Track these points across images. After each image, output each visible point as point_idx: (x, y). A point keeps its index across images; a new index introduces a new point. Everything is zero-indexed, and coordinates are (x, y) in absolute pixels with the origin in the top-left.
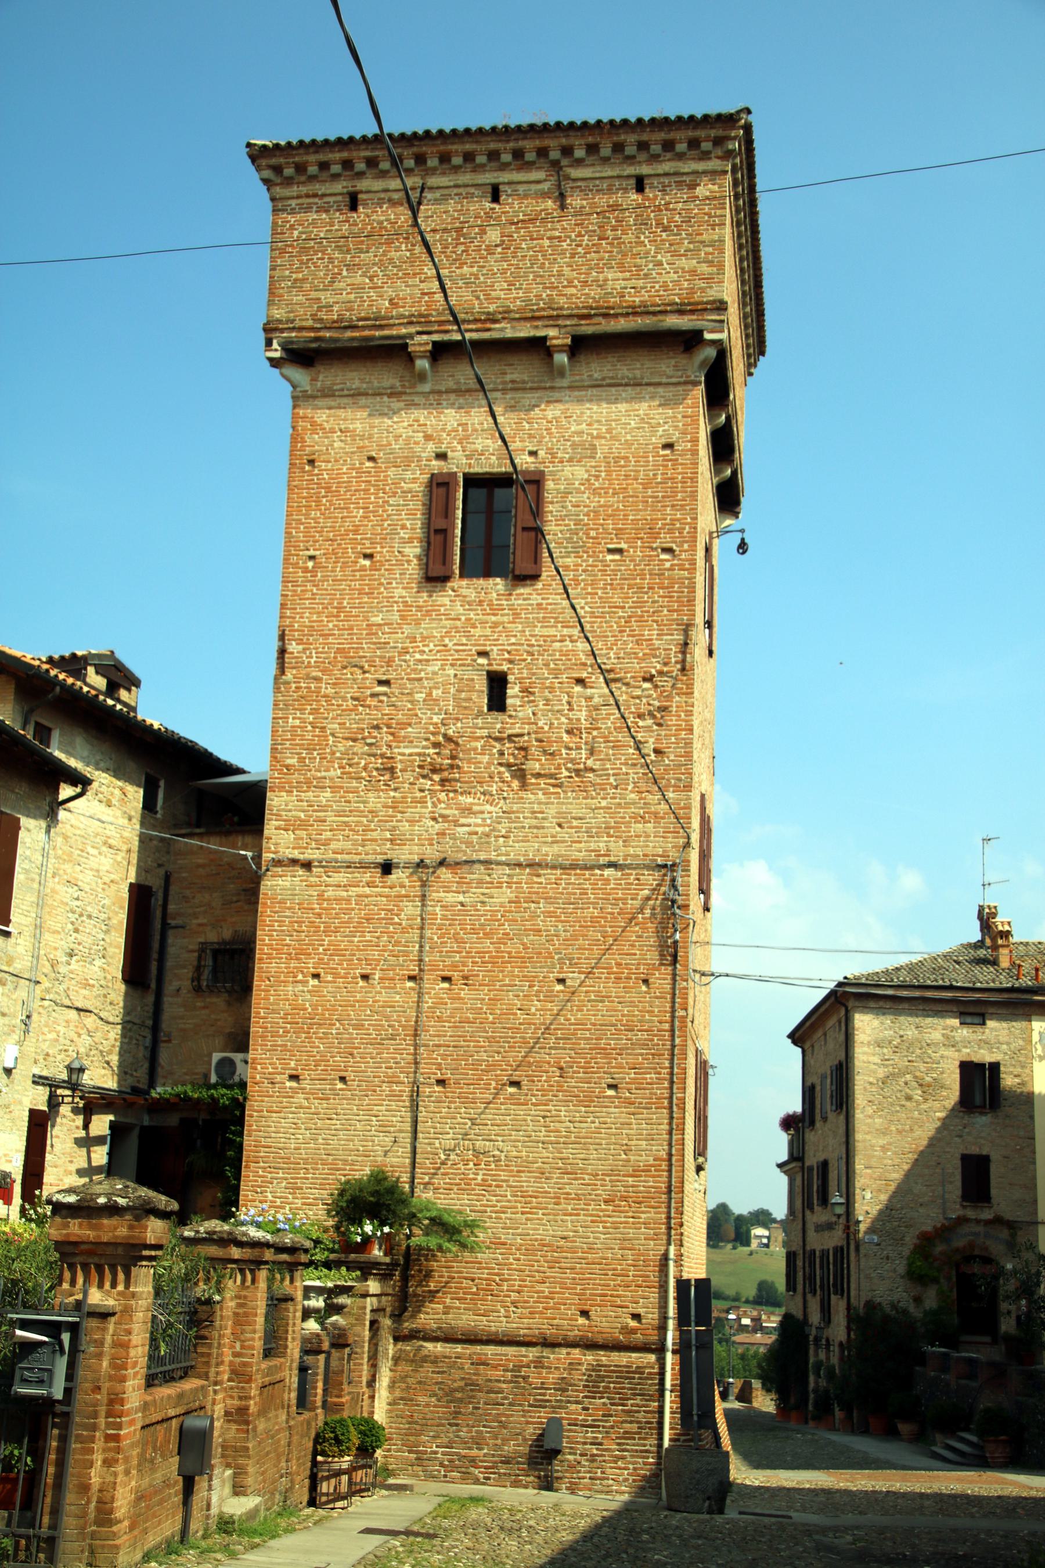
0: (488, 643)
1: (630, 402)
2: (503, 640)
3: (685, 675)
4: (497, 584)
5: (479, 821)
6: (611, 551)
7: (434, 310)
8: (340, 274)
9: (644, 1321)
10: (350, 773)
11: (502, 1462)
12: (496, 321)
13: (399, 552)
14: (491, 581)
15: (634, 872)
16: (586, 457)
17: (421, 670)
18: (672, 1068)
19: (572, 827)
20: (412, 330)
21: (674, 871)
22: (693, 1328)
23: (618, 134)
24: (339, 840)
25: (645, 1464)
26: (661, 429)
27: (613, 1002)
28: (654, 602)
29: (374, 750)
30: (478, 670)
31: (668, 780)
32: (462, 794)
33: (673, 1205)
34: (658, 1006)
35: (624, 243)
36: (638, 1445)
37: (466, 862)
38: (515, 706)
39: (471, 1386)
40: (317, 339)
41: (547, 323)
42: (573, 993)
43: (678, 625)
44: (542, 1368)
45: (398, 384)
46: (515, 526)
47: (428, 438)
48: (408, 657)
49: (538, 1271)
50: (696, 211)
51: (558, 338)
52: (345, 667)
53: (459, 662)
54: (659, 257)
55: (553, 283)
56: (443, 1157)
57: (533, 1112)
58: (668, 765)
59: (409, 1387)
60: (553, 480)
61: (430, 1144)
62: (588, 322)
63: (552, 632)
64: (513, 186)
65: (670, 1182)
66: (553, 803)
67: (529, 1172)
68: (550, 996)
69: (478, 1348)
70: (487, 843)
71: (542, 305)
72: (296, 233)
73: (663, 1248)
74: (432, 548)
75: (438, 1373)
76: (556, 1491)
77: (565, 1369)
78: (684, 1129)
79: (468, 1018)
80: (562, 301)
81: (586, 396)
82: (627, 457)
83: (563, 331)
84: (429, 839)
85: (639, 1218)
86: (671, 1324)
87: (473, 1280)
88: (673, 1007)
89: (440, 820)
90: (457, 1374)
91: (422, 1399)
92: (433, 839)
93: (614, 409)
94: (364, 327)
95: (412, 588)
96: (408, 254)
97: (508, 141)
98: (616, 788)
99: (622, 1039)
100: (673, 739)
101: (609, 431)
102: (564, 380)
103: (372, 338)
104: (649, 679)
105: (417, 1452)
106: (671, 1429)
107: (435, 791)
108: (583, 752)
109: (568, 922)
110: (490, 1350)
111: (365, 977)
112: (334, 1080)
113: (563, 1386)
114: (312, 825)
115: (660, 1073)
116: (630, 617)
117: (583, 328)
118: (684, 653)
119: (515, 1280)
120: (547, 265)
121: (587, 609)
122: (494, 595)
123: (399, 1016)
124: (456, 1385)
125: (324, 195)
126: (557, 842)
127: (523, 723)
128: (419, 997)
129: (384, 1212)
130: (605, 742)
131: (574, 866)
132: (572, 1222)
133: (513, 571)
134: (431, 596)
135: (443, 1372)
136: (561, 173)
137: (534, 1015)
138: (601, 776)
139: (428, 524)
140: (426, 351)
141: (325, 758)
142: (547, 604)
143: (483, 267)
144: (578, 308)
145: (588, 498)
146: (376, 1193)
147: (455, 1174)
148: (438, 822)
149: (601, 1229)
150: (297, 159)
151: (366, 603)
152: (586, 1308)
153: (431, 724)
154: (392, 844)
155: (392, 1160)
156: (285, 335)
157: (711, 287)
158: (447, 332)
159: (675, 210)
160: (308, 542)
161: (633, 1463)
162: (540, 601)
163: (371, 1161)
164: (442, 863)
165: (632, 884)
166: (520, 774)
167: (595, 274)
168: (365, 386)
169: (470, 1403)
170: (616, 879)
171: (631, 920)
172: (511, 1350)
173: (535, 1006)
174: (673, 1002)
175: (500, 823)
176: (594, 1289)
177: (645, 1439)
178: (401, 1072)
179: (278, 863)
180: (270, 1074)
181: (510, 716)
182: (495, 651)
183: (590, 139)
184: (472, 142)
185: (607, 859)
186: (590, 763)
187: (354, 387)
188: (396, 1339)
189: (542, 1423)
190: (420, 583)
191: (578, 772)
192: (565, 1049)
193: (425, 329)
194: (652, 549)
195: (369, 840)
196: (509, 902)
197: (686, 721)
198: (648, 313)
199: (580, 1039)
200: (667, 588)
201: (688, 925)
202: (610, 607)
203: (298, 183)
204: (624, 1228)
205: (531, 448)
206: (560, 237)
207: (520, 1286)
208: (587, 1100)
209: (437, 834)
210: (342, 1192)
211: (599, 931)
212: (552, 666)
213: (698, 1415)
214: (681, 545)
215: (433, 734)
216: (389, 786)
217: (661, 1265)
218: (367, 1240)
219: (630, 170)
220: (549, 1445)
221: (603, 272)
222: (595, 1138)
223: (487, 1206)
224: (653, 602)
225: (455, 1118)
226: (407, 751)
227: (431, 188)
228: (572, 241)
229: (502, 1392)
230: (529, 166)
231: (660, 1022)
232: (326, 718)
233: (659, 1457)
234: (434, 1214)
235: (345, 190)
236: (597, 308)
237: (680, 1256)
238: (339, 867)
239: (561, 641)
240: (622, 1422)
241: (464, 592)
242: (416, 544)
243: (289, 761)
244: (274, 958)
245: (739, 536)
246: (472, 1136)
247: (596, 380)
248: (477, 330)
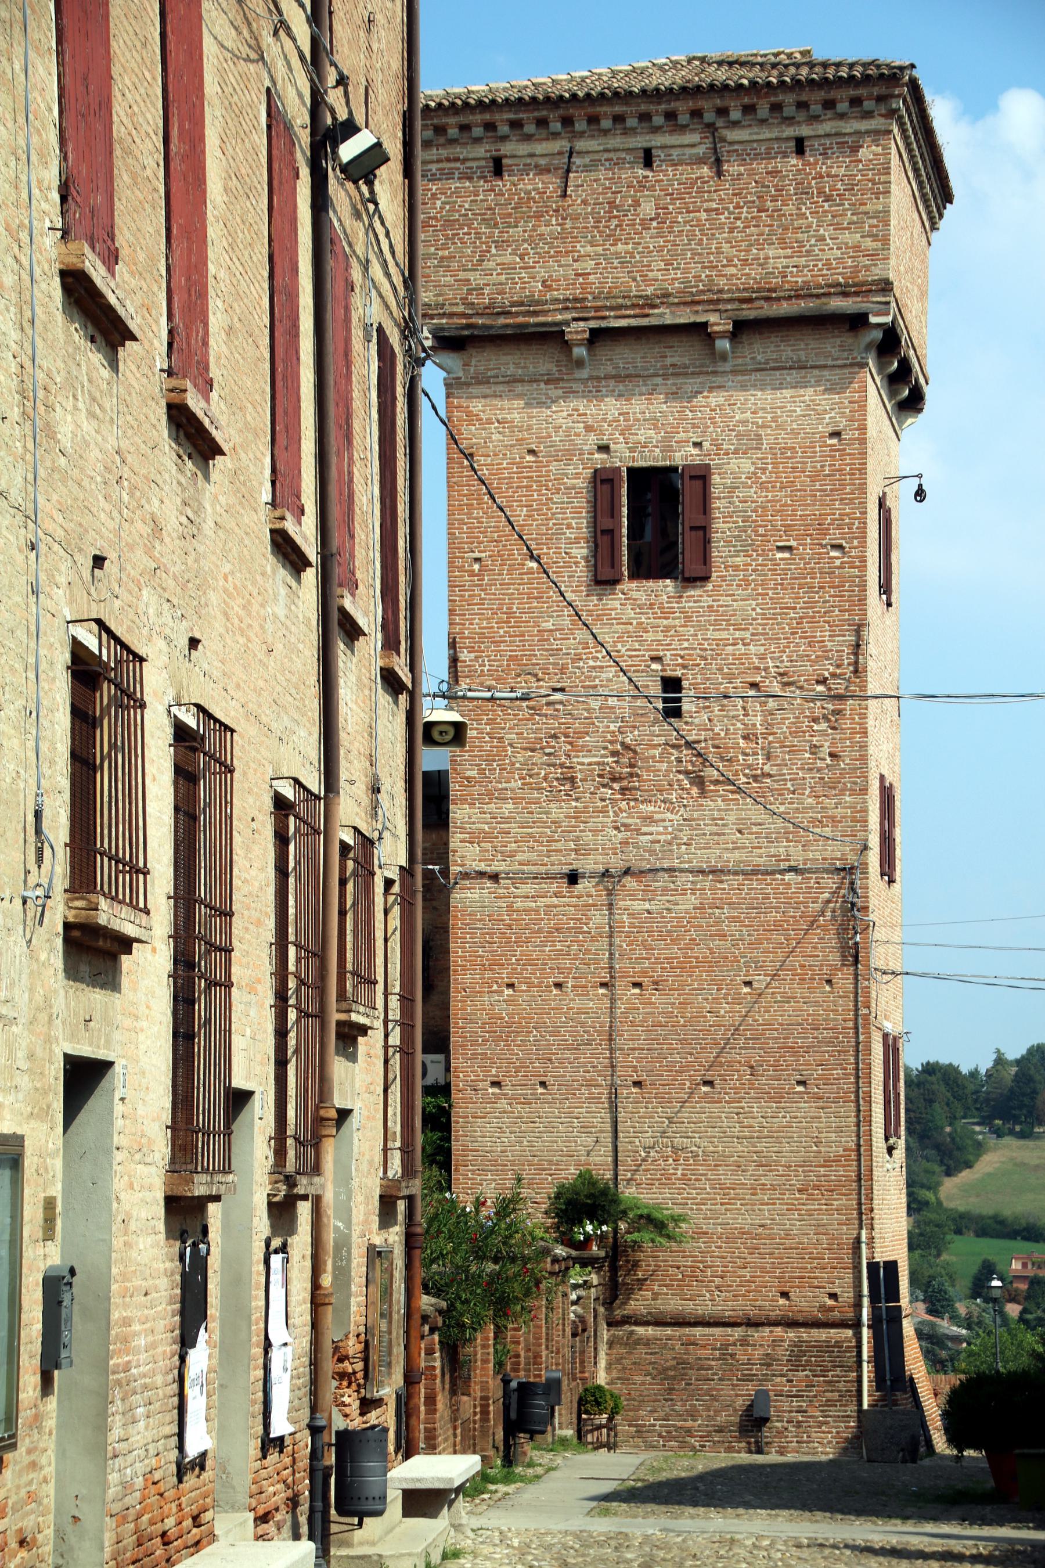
0: (661, 648)
1: (795, 387)
4: (667, 586)
5: (661, 829)
6: (781, 549)
7: (589, 293)
9: (840, 1300)
11: (715, 1431)
13: (566, 553)
14: (661, 582)
15: (814, 876)
16: (752, 449)
17: (596, 677)
18: (857, 1063)
19: (752, 833)
20: (568, 316)
21: (852, 874)
22: (883, 1305)
23: (776, 95)
24: (524, 852)
26: (827, 416)
27: (798, 1002)
29: (553, 760)
31: (844, 784)
32: (642, 802)
33: (863, 1192)
34: (842, 1005)
35: (784, 215)
36: (839, 1411)
37: (651, 870)
38: (691, 712)
39: (682, 1363)
40: (469, 326)
41: (707, 307)
42: (760, 995)
43: (849, 625)
44: (748, 1345)
45: (555, 369)
47: (589, 429)
48: (581, 664)
50: (859, 177)
51: (719, 324)
52: (519, 675)
53: (632, 669)
54: (822, 231)
56: (643, 1154)
58: (844, 769)
59: (624, 1369)
62: (749, 306)
63: (724, 635)
64: (666, 150)
65: (859, 1170)
66: (732, 810)
67: (726, 1165)
68: (738, 999)
69: (687, 1330)
70: (670, 850)
71: (701, 287)
72: (439, 203)
73: (855, 1232)
74: (599, 550)
75: (651, 1354)
76: (768, 1454)
78: (870, 1121)
80: (722, 282)
81: (750, 380)
82: (794, 448)
83: (724, 315)
84: (613, 849)
85: (832, 1205)
86: (866, 1301)
87: (678, 1268)
88: (856, 1005)
89: (623, 829)
90: (668, 1354)
92: (616, 848)
94: (518, 314)
95: (582, 591)
96: (559, 229)
97: (659, 104)
98: (793, 793)
99: (808, 1038)
100: (848, 743)
101: (774, 419)
102: (727, 364)
103: (527, 325)
104: (823, 681)
105: (636, 1426)
106: (869, 1396)
108: (760, 757)
110: (698, 1331)
111: (558, 985)
112: (535, 1085)
113: (768, 1361)
114: (497, 837)
116: (801, 618)
117: (745, 313)
118: (856, 654)
119: (718, 1266)
120: (705, 241)
121: (759, 610)
122: (665, 597)
123: (593, 1022)
124: (668, 1364)
125: (465, 160)
126: (738, 848)
128: (612, 1003)
130: (781, 747)
131: (755, 872)
132: (769, 1210)
134: (601, 600)
135: (655, 1353)
136: (716, 134)
137: (724, 1017)
138: (779, 781)
139: (594, 523)
140: (583, 340)
141: (505, 769)
142: (718, 606)
143: (639, 244)
144: (738, 289)
145: (756, 493)
147: (656, 1170)
148: (620, 831)
149: (796, 1216)
150: (435, 121)
151: (536, 608)
152: (786, 1289)
153: (608, 732)
155: (594, 1159)
156: (435, 321)
157: (876, 265)
158: (604, 318)
160: (473, 543)
162: (711, 603)
163: (575, 1161)
164: (627, 872)
165: (812, 888)
166: (699, 782)
167: (755, 251)
168: (520, 372)
169: (682, 1380)
170: (796, 884)
171: (812, 923)
172: (717, 1331)
173: (724, 1008)
174: (856, 1001)
175: (681, 831)
177: (845, 1406)
178: (599, 1076)
179: (466, 876)
180: (472, 1081)
181: (686, 723)
182: (669, 657)
183: (746, 100)
184: (622, 104)
185: (787, 863)
186: (767, 768)
187: (509, 373)
189: (750, 1395)
190: (588, 586)
191: (755, 778)
192: (754, 1048)
193: (581, 315)
196: (694, 909)
197: (860, 724)
198: (811, 296)
199: (768, 1038)
200: (838, 587)
201: (868, 926)
202: (781, 608)
203: (438, 146)
205: (695, 440)
206: (717, 209)
207: (722, 1271)
208: (778, 1096)
209: (620, 843)
211: (782, 935)
212: (726, 670)
213: (891, 1381)
215: (611, 742)
216: (570, 796)
217: (854, 1248)
219: (790, 132)
220: (757, 1413)
221: (764, 249)
222: (787, 1132)
224: (824, 602)
225: (653, 1117)
226: (586, 760)
229: (712, 1369)
230: (683, 128)
232: (504, 729)
235: (488, 155)
236: (758, 291)
237: (871, 1239)
238: (526, 878)
239: (733, 645)
241: (634, 594)
242: (582, 545)
243: (469, 773)
244: (469, 970)
245: (917, 481)
248: (635, 316)
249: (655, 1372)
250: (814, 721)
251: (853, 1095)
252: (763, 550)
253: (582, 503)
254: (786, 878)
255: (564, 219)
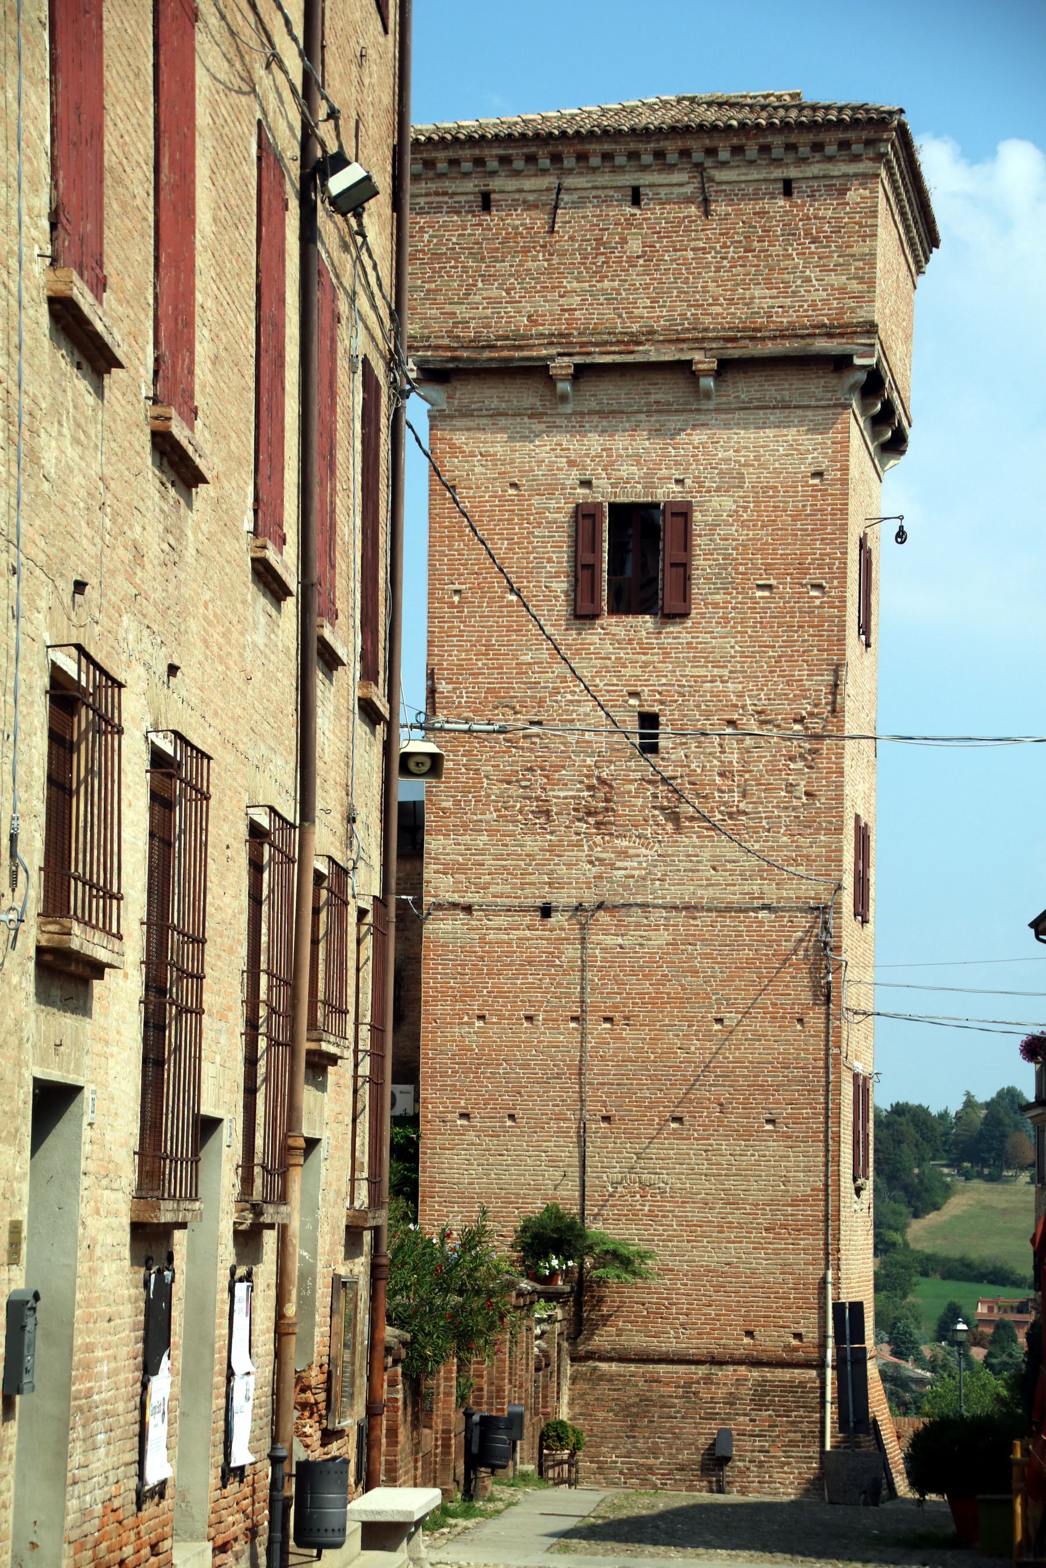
1: (778, 427)
2: (653, 680)
3: (835, 717)
4: (646, 622)
5: (635, 864)
6: (760, 587)
7: (575, 329)
8: (475, 285)
9: (805, 1340)
10: (506, 816)
11: (677, 1469)
12: (639, 343)
13: (546, 587)
14: (640, 618)
15: (787, 915)
16: (733, 487)
18: (827, 1103)
19: (726, 871)
20: (553, 351)
21: (826, 913)
22: (847, 1346)
23: (765, 137)
24: (498, 884)
25: (809, 1468)
26: (810, 456)
27: (769, 1040)
28: (803, 641)
30: (629, 711)
32: (617, 837)
33: (830, 1232)
34: (813, 1045)
35: (771, 256)
36: (802, 1452)
37: (624, 905)
40: (453, 359)
42: (731, 1032)
43: (828, 665)
44: (711, 1384)
45: (539, 403)
46: (663, 560)
47: (571, 463)
49: (705, 1295)
50: (846, 220)
51: (704, 362)
52: (497, 708)
53: (610, 703)
54: (808, 273)
55: (697, 300)
56: (611, 1189)
57: (695, 1147)
58: (819, 808)
60: (701, 511)
61: (598, 1177)
62: (734, 345)
63: (702, 672)
64: (654, 188)
65: (827, 1210)
66: (707, 846)
68: (709, 1036)
69: (651, 1367)
70: (644, 886)
71: (687, 326)
73: (822, 1272)
74: (579, 584)
75: (614, 1390)
77: (732, 1385)
78: (839, 1161)
79: (631, 1057)
81: (733, 419)
82: (776, 487)
83: (709, 354)
85: (799, 1244)
86: (830, 1342)
88: (827, 1045)
89: (597, 863)
91: (601, 1415)
92: (590, 883)
93: (762, 434)
94: (503, 348)
95: (561, 625)
96: (546, 264)
97: (648, 142)
98: (768, 831)
99: (778, 1076)
100: (824, 782)
101: (757, 458)
102: (711, 402)
103: (512, 359)
105: (598, 1462)
106: (832, 1437)
107: (592, 834)
108: (736, 794)
109: (725, 963)
110: (662, 1369)
111: (529, 1018)
112: (503, 1117)
113: (731, 1400)
114: (471, 869)
115: (815, 1108)
116: (780, 656)
117: (730, 352)
118: (834, 694)
119: (683, 1303)
120: (691, 280)
121: (737, 648)
122: (644, 633)
125: (455, 194)
126: (712, 885)
127: (675, 766)
129: (566, 1247)
130: (757, 785)
131: (728, 909)
133: (662, 608)
134: (580, 634)
135: (618, 1390)
136: (705, 174)
137: (694, 1053)
138: (754, 818)
140: (568, 375)
143: (626, 281)
144: (723, 329)
145: (737, 531)
146: (557, 1230)
148: (594, 866)
149: (763, 1255)
150: (425, 155)
151: (515, 640)
152: (751, 1328)
153: (584, 766)
154: (550, 887)
155: (562, 1193)
156: (420, 353)
157: (861, 307)
158: (589, 354)
159: (825, 218)
161: (798, 1468)
162: (690, 640)
163: (542, 1194)
164: (600, 906)
165: (785, 926)
166: (674, 818)
167: (741, 291)
168: (504, 405)
169: (645, 1417)
171: (785, 961)
172: (681, 1369)
173: (695, 1045)
174: (827, 1041)
175: (656, 866)
176: (757, 1311)
177: (808, 1447)
179: (439, 907)
180: (440, 1112)
181: (663, 759)
182: (646, 692)
183: (735, 141)
186: (742, 806)
188: (573, 1360)
189: (713, 1434)
190: (568, 620)
192: (724, 1086)
193: (566, 350)
194: (803, 586)
195: (527, 884)
196: (667, 944)
197: (836, 764)
198: (796, 336)
200: (817, 626)
201: (841, 966)
202: (760, 646)
203: (427, 180)
204: (785, 1254)
205: (677, 477)
206: (704, 248)
207: (687, 1309)
208: (747, 1134)
209: (594, 877)
210: (524, 1229)
212: (703, 707)
213: (855, 1423)
214: (830, 582)
216: (545, 829)
218: (554, 1272)
219: (778, 173)
220: (719, 1452)
221: (749, 289)
222: (755, 1170)
223: (655, 1235)
224: (803, 641)
225: (621, 1153)
226: (562, 794)
227: (568, 190)
228: (717, 252)
229: (675, 1407)
230: (671, 168)
231: (815, 1060)
232: (480, 760)
233: (822, 1462)
234: (611, 1247)
235: (477, 189)
237: (837, 1280)
238: (499, 910)
240: (787, 1432)
241: (614, 630)
242: (563, 579)
243: (444, 804)
246: (638, 1170)
247: (743, 402)
248: (620, 353)
249: (617, 1408)
250: (790, 759)
251: (822, 1135)
252: (743, 588)
253: (562, 537)
254: (760, 915)
255: (551, 254)
